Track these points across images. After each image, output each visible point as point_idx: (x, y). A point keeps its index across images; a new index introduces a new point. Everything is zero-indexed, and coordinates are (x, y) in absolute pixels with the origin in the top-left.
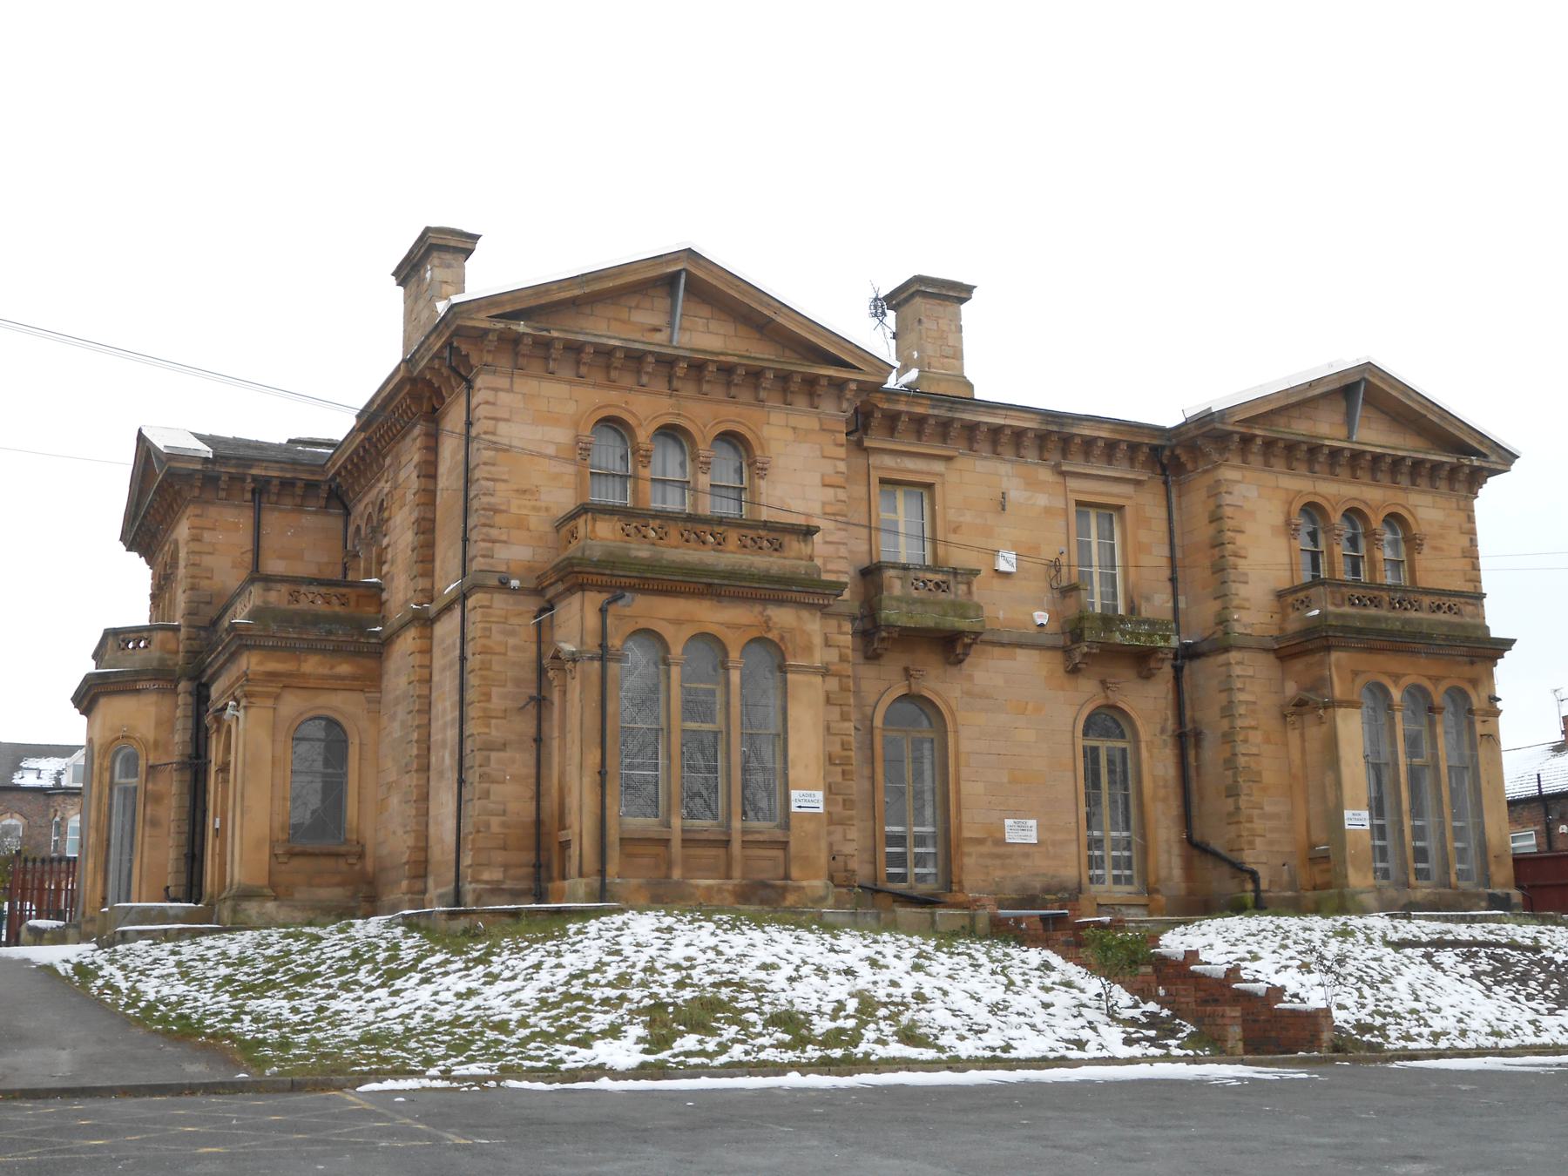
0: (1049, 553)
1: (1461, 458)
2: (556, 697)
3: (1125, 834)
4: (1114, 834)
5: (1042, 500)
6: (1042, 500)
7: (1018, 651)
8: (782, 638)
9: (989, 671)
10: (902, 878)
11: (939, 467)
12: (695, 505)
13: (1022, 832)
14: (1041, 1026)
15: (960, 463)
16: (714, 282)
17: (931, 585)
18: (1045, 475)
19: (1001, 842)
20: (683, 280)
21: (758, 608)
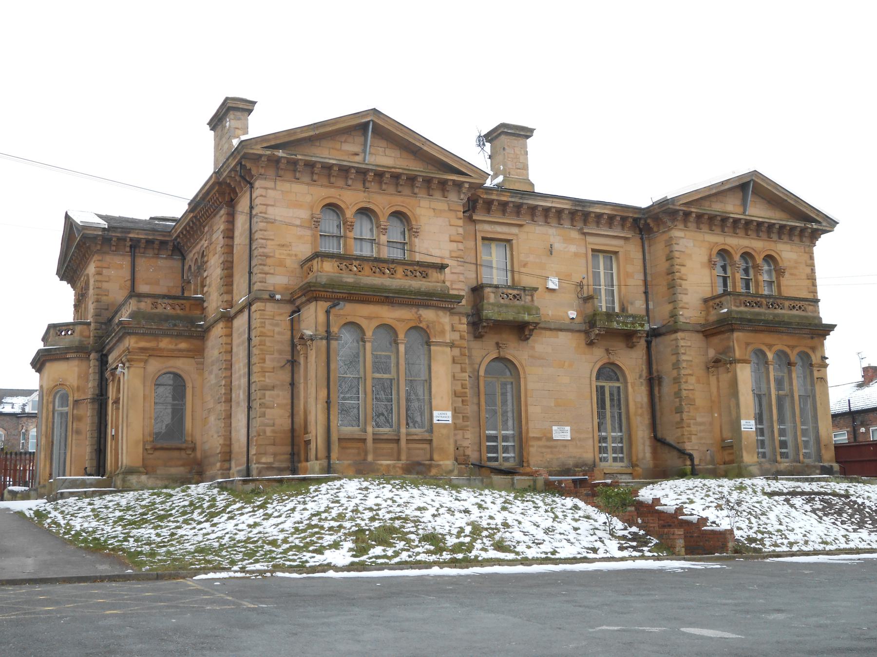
0: (577, 278)
3: (619, 434)
5: (573, 248)
7: (560, 333)
11: (515, 230)
13: (562, 433)
17: (511, 297)
18: (574, 234)
19: (550, 439)
21: (414, 310)
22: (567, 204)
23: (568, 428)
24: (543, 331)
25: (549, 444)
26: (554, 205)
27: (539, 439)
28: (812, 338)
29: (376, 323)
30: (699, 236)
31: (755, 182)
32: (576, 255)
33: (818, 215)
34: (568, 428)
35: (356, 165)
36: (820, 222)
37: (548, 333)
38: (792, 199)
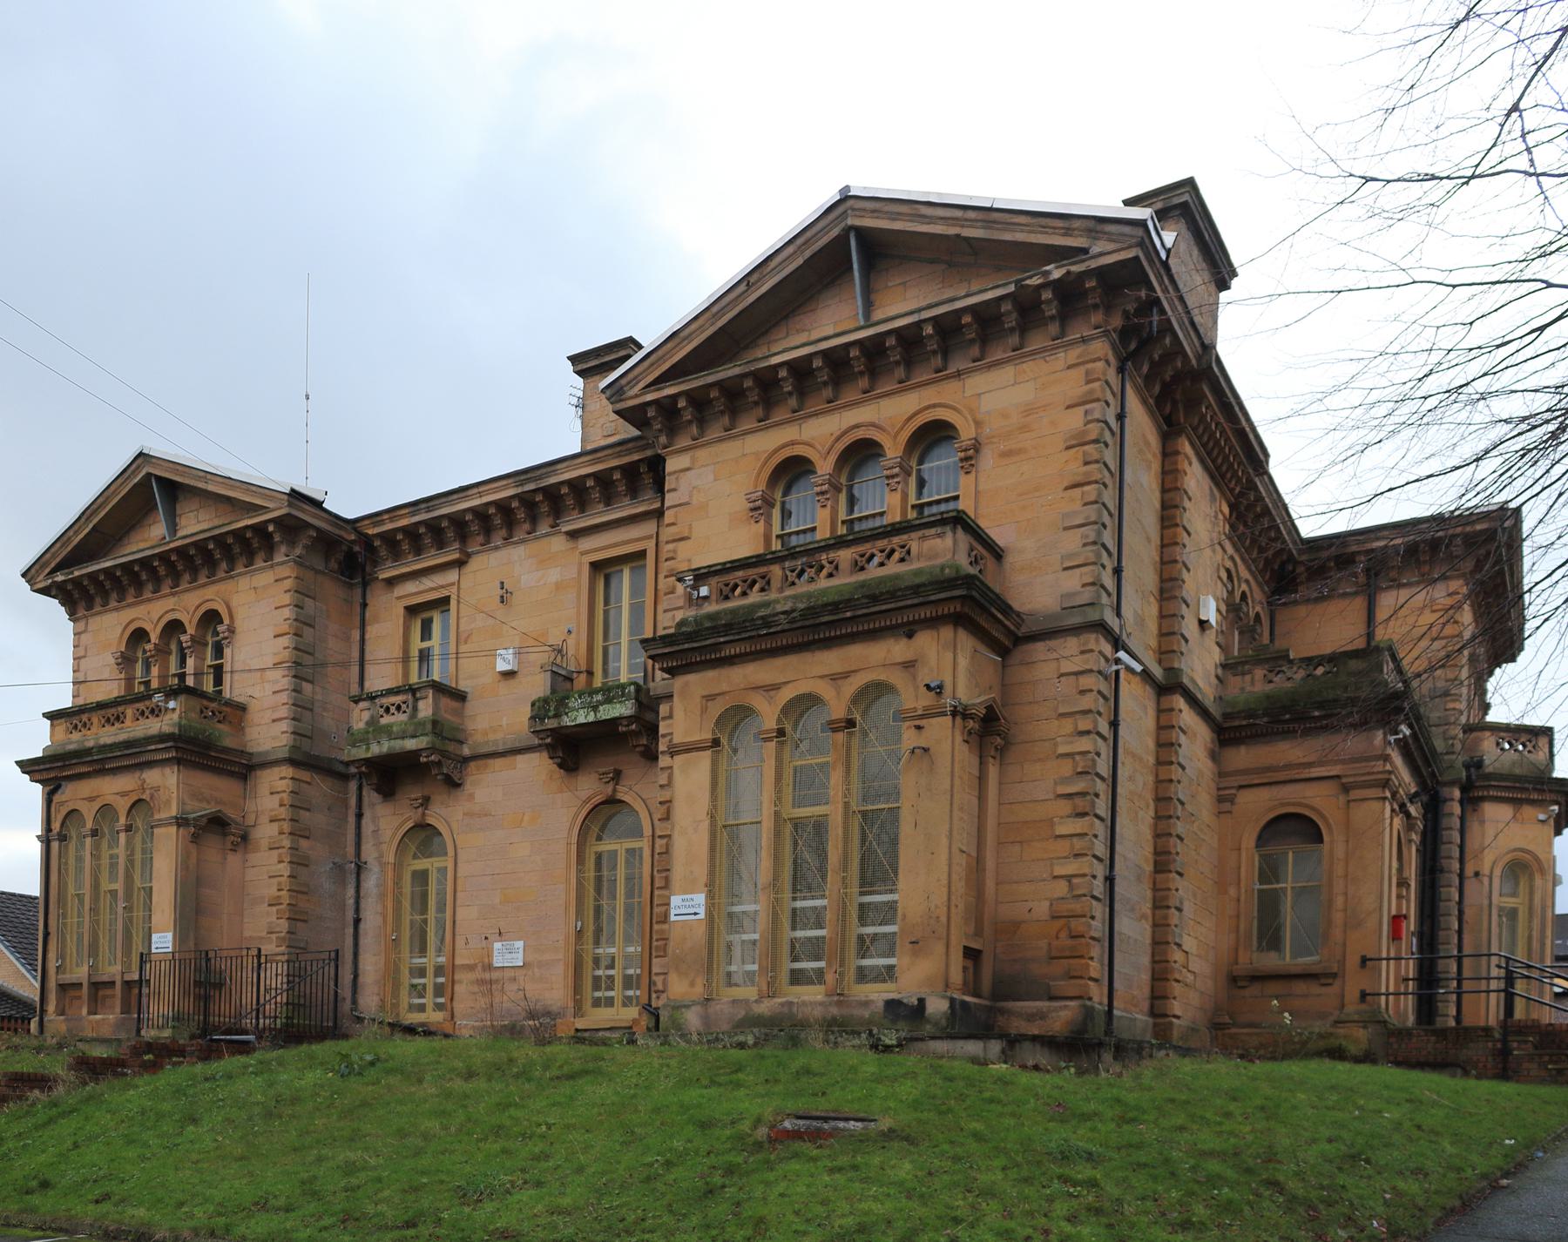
0: (555, 638)
1: (1128, 299)
2: (959, 887)
3: (600, 951)
4: (613, 950)
5: (554, 575)
6: (554, 575)
7: (519, 758)
8: (152, 797)
9: (490, 788)
10: (422, 1008)
11: (452, 576)
12: (387, 661)
13: (508, 954)
14: (802, 1228)
15: (475, 563)
16: (898, 226)
17: (393, 709)
18: (558, 543)
19: (489, 967)
20: (855, 243)
21: (137, 774)
22: (506, 487)
23: (520, 944)
24: (490, 761)
25: (487, 976)
26: (485, 499)
27: (471, 968)
28: (910, 636)
29: (96, 805)
30: (732, 449)
31: (861, 233)
32: (558, 587)
33: (1068, 232)
34: (520, 944)
35: (157, 551)
36: (1085, 251)
37: (499, 762)
38: (972, 223)
